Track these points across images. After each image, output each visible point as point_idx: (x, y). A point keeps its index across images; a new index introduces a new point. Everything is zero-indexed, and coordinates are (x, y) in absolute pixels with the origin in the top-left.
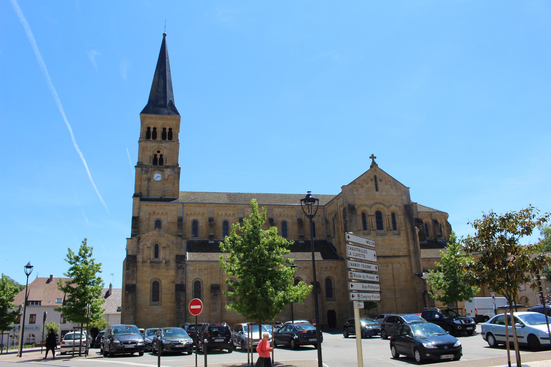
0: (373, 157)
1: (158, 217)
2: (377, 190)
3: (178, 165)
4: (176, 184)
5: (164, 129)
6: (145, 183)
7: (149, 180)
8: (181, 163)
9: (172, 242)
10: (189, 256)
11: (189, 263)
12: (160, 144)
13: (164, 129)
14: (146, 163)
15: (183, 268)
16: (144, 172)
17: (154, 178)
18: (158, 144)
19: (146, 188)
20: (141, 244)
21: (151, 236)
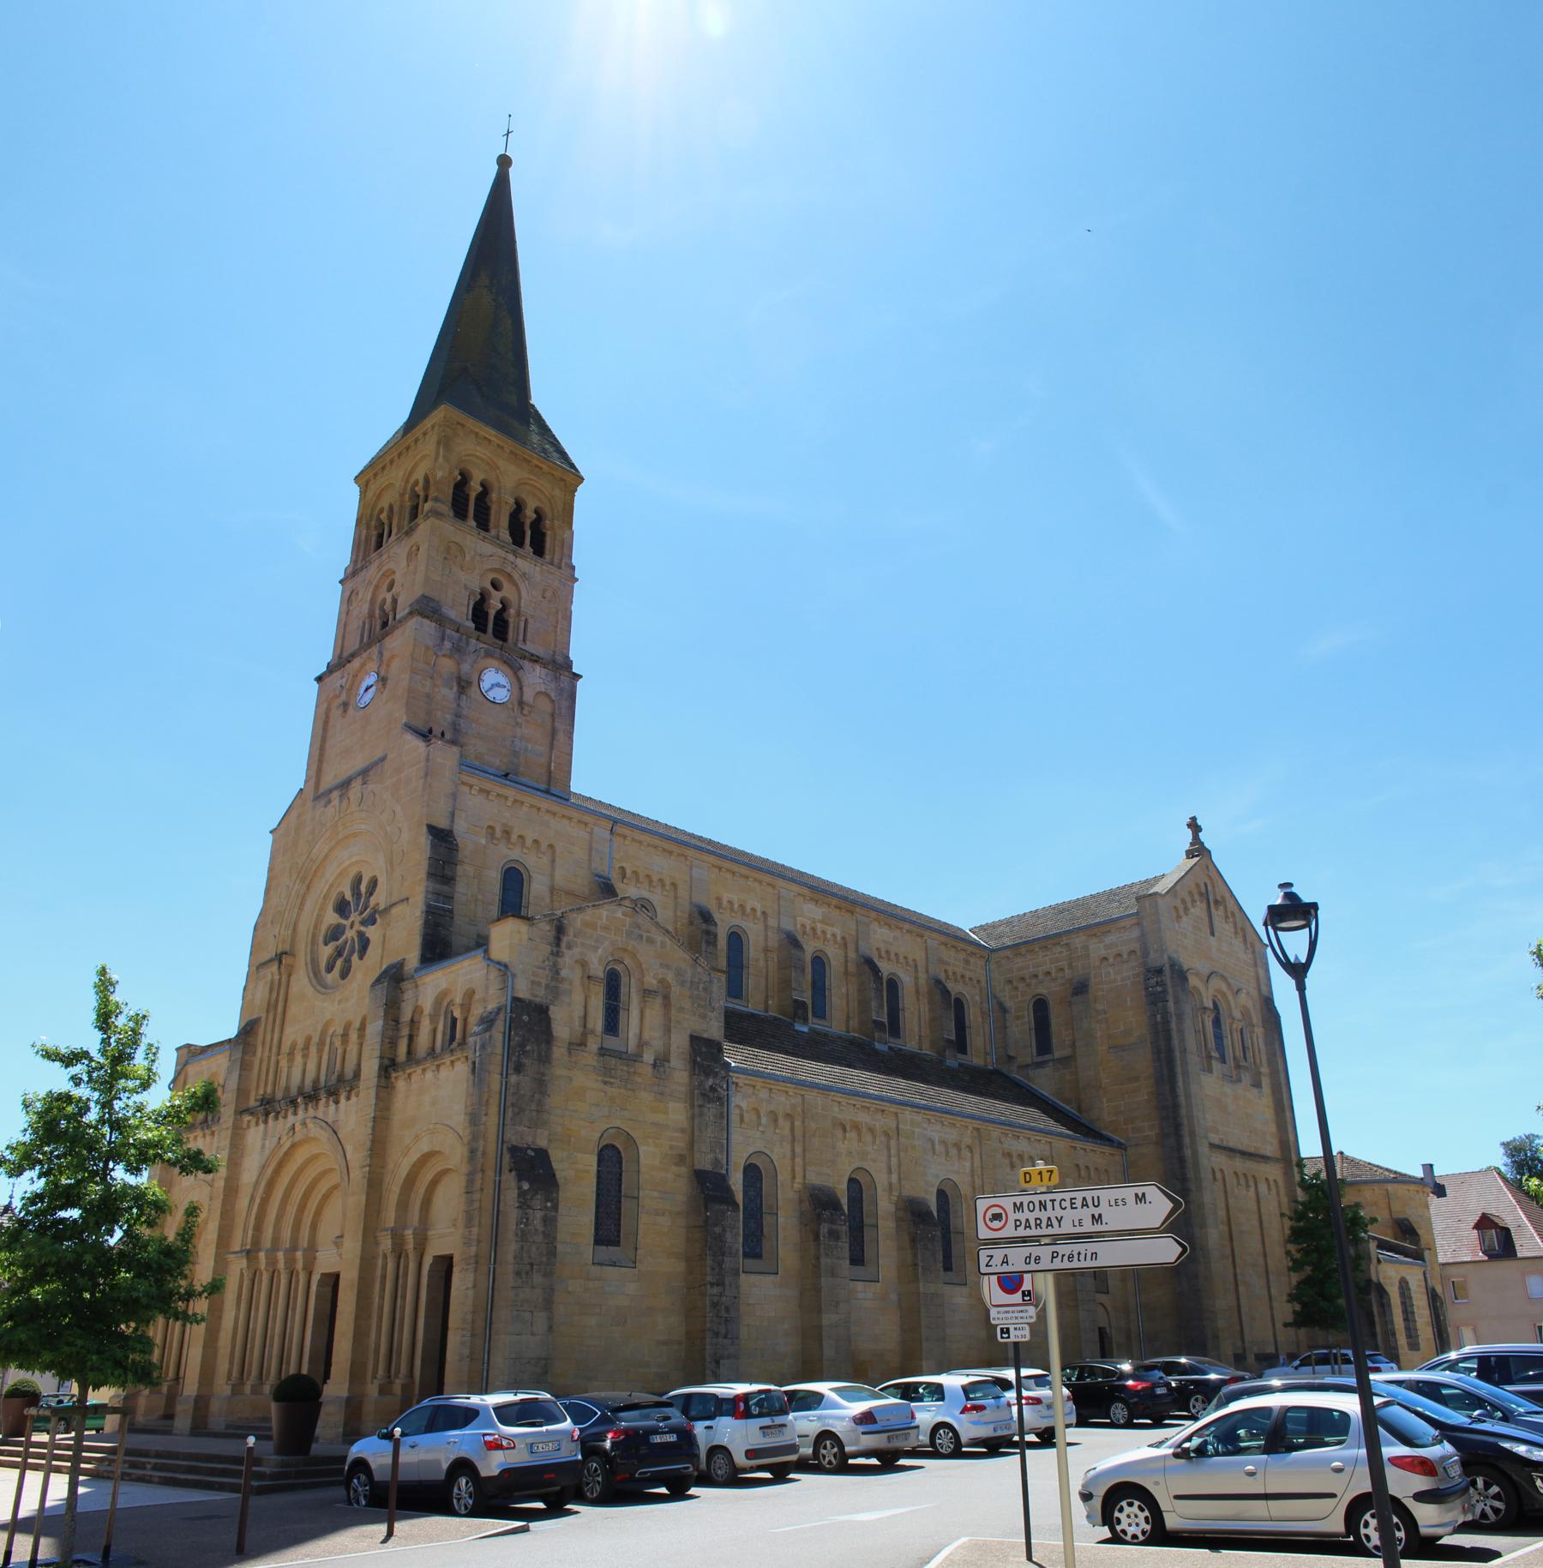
0: (1194, 826)
1: (515, 854)
2: (1212, 934)
3: (569, 664)
4: (561, 737)
5: (519, 507)
6: (448, 693)
7: (464, 685)
8: (580, 655)
9: (679, 973)
10: (734, 1056)
11: (741, 1079)
12: (511, 557)
13: (519, 507)
14: (452, 614)
15: (719, 1099)
16: (448, 644)
17: (485, 685)
18: (501, 553)
19: (449, 717)
20: (568, 958)
21: (606, 928)
